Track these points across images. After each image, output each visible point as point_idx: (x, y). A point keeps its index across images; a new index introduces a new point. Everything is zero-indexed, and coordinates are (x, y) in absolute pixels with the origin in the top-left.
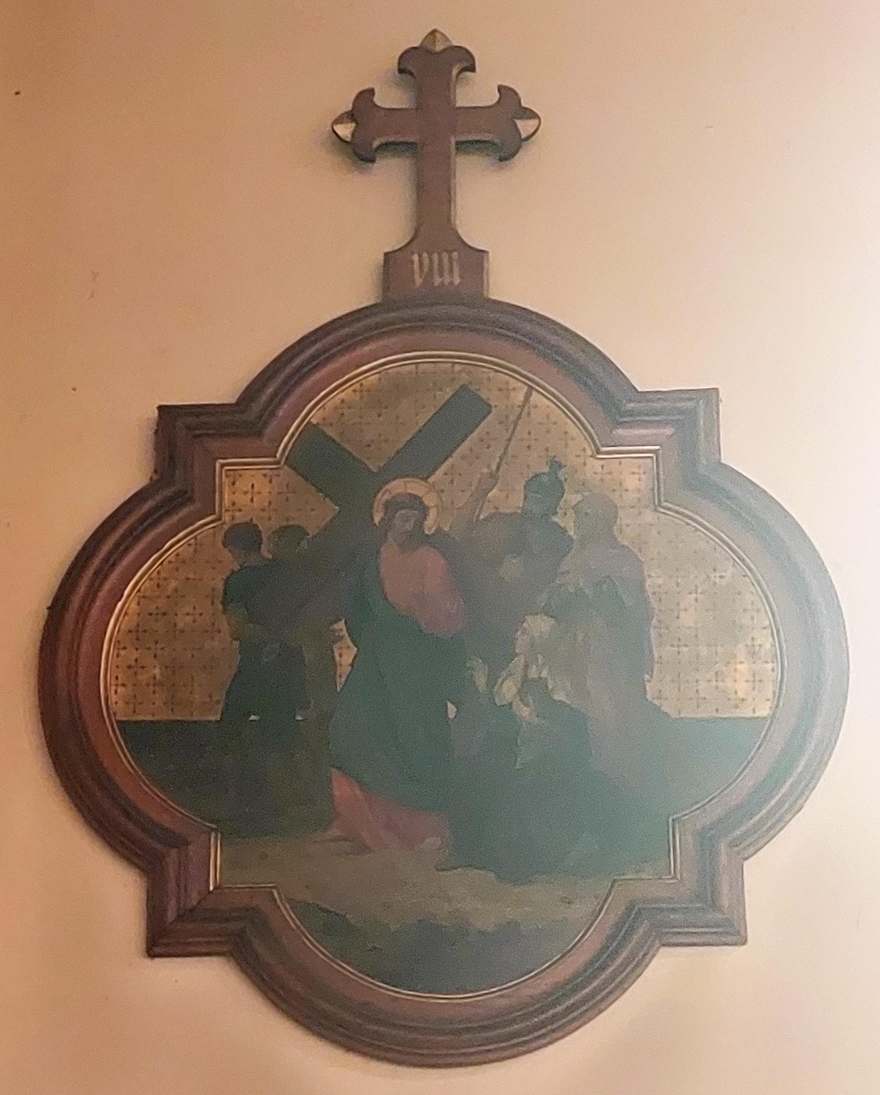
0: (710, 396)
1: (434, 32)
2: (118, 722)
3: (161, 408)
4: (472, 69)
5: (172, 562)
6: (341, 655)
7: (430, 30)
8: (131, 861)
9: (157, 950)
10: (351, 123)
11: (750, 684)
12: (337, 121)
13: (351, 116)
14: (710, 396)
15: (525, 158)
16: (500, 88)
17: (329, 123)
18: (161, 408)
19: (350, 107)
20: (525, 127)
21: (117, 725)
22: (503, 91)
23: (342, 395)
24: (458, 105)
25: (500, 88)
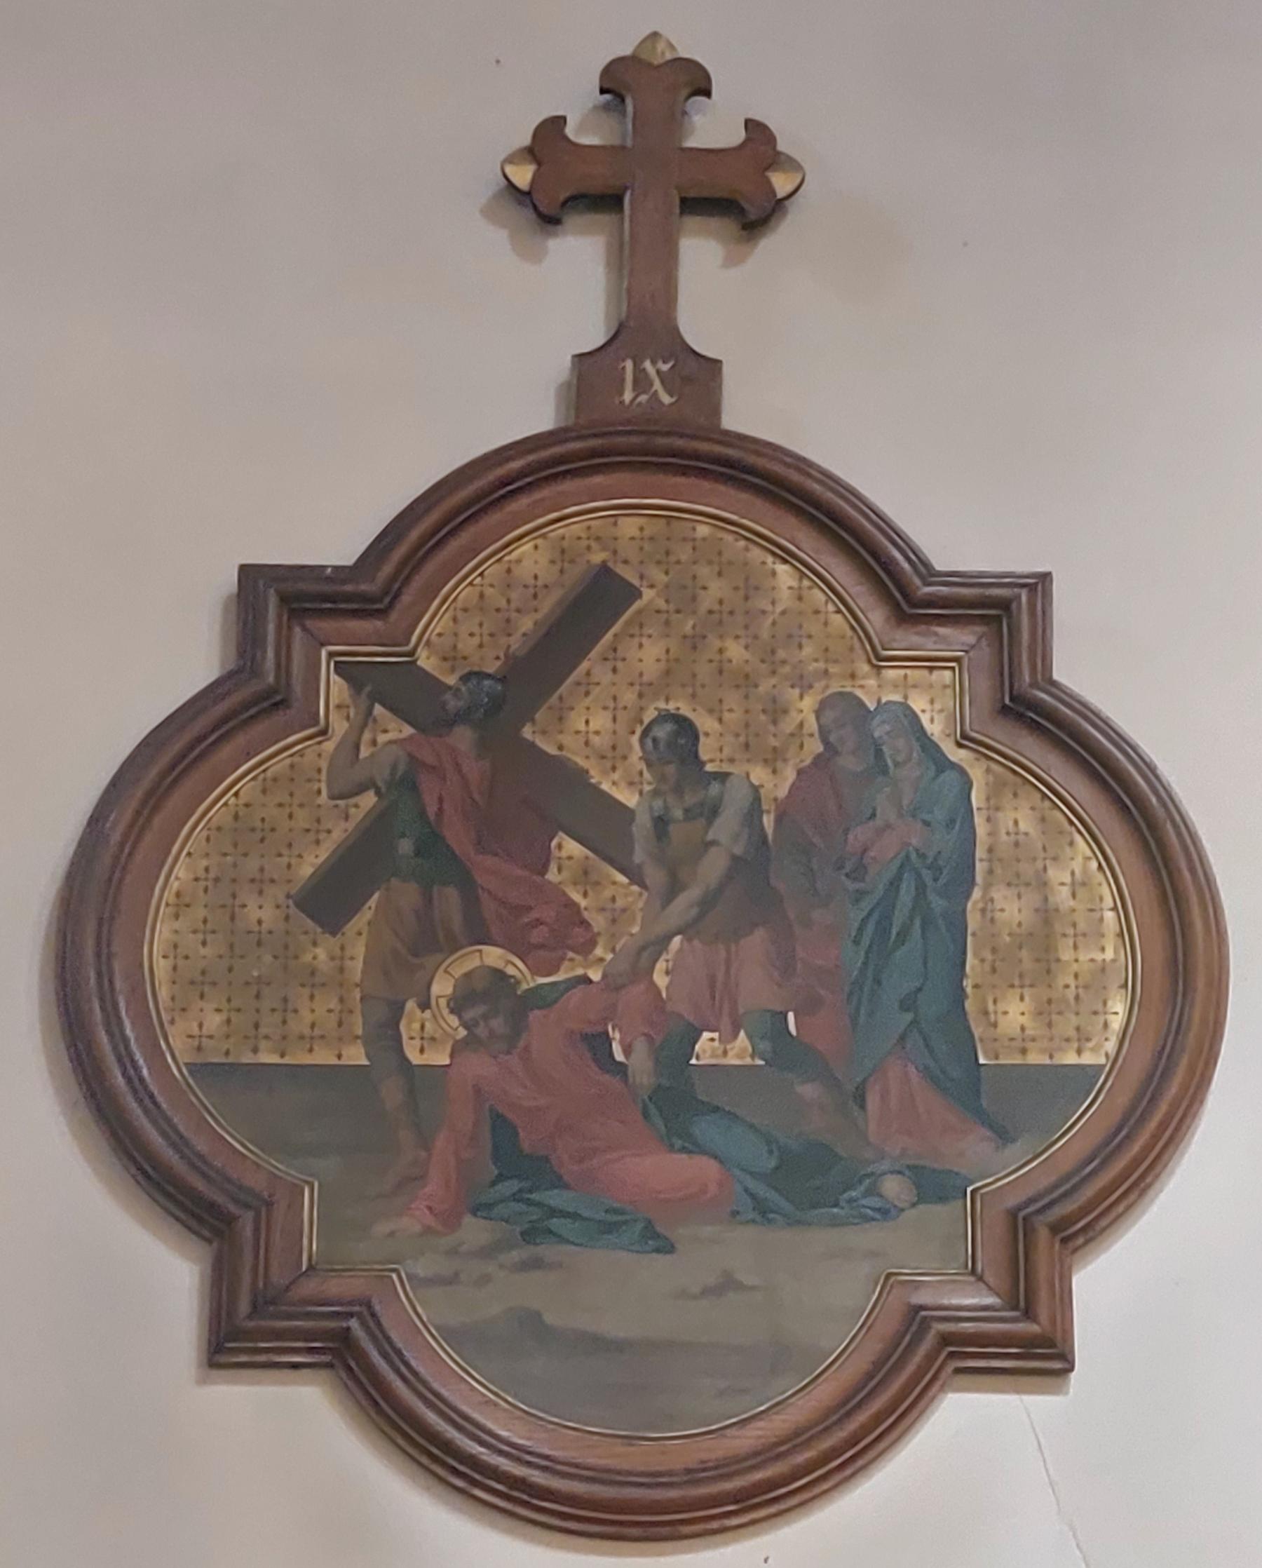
0: (1040, 584)
1: (655, 35)
2: (186, 1064)
3: (244, 569)
4: (707, 93)
5: (210, 983)
6: (995, 1002)
7: (648, 32)
8: (226, 694)
9: (223, 1359)
10: (530, 163)
11: (316, 993)
12: (510, 160)
13: (531, 153)
14: (1040, 584)
15: (771, 244)
16: (748, 123)
17: (503, 157)
18: (244, 569)
19: (526, 140)
20: (781, 183)
21: (187, 1068)
22: (750, 125)
23: (561, 531)
24: (691, 143)
25: (748, 123)
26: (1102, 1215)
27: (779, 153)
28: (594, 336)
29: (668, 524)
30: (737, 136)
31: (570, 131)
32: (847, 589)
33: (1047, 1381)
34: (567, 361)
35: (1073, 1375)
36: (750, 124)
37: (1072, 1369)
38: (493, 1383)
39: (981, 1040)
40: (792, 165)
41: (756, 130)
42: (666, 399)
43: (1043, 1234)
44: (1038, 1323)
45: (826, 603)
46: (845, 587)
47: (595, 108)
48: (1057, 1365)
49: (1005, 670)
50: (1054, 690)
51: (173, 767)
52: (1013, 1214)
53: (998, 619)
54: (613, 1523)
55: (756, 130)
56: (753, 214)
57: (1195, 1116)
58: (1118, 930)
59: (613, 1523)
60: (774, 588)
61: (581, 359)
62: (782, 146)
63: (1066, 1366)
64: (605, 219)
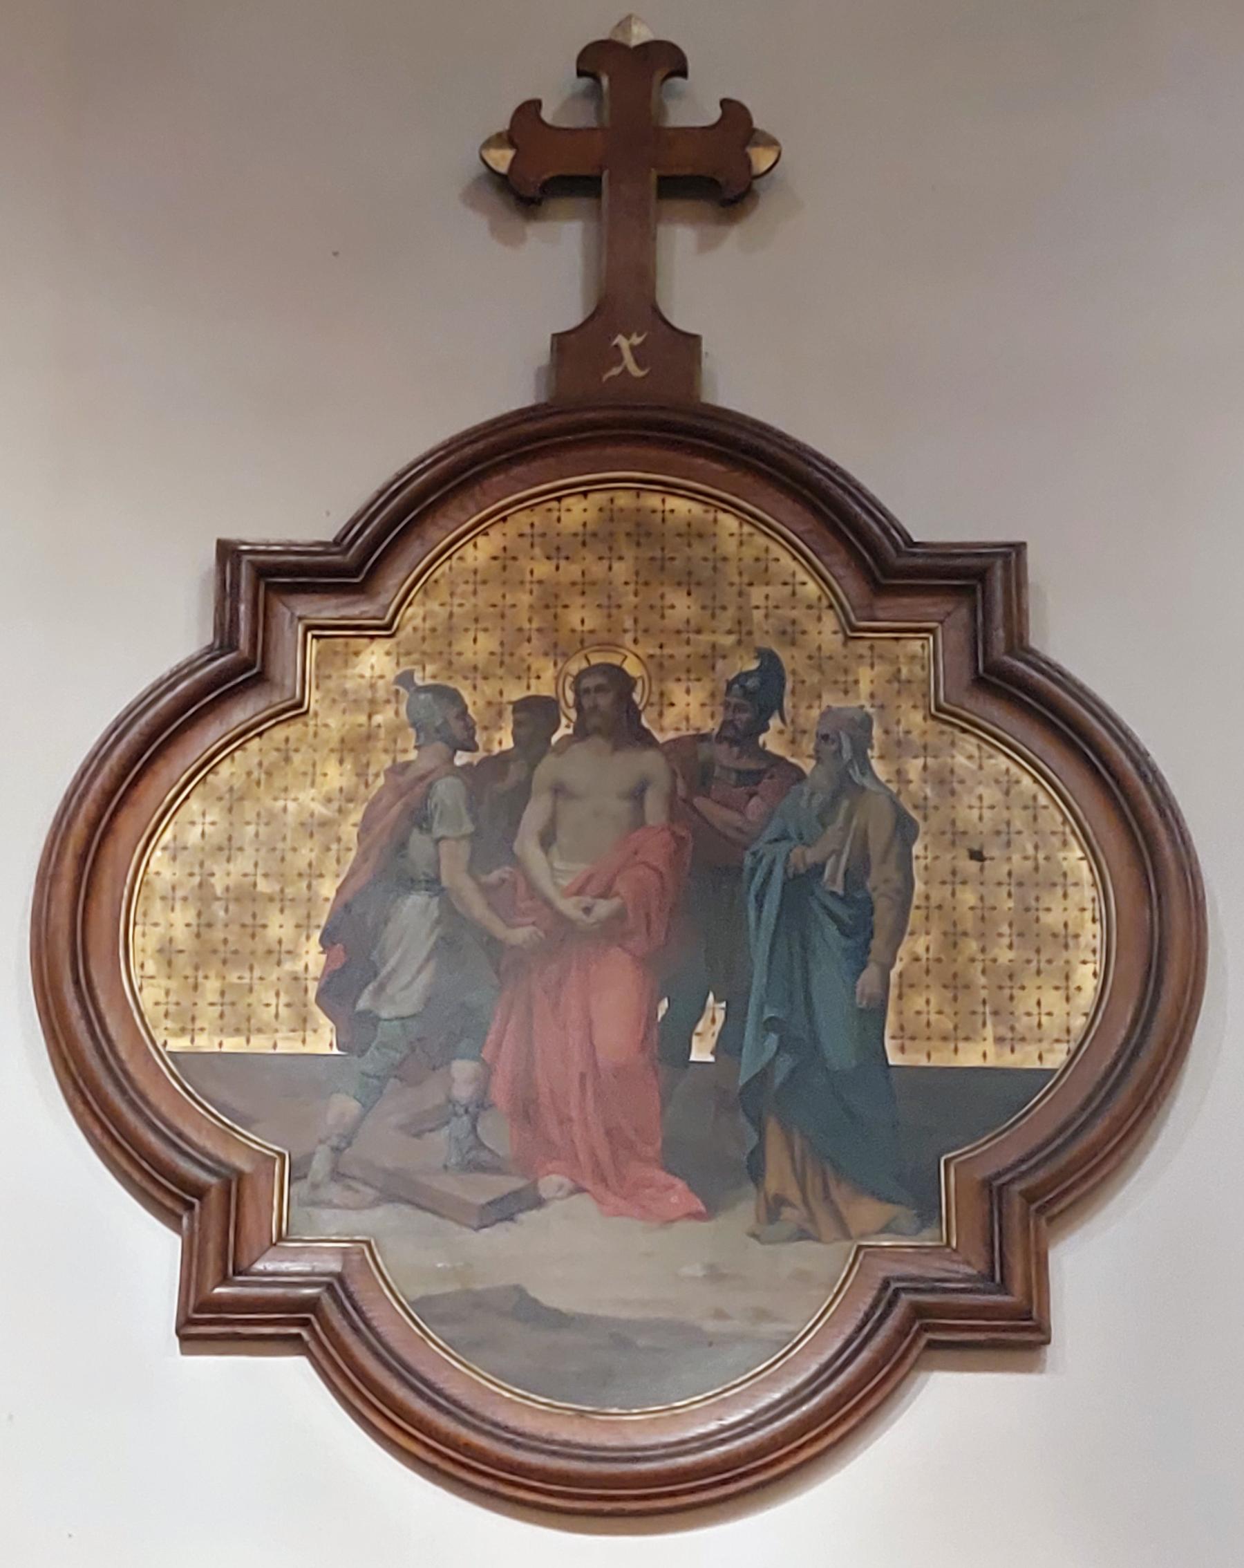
4: (683, 73)
12: (488, 144)
13: (507, 139)
26: (1085, 1177)
27: (754, 131)
28: (571, 315)
29: (638, 496)
30: (713, 114)
31: (547, 115)
32: (1059, 775)
33: (1018, 1356)
34: (546, 344)
35: (1049, 1349)
36: (725, 103)
37: (1048, 1342)
38: (517, 1387)
39: (176, 823)
40: (772, 142)
41: (733, 111)
42: (636, 372)
43: (1016, 1206)
44: (1013, 1295)
45: (741, 525)
46: (1026, 744)
47: (574, 97)
48: (1042, 1338)
49: (978, 639)
50: (1030, 657)
51: (126, 770)
52: (987, 1183)
53: (973, 590)
54: (856, 1408)
55: (733, 111)
56: (729, 195)
57: (1176, 1075)
58: (527, 512)
59: (856, 1408)
60: (715, 535)
61: (560, 341)
62: (758, 123)
63: (1042, 1338)
64: (585, 203)
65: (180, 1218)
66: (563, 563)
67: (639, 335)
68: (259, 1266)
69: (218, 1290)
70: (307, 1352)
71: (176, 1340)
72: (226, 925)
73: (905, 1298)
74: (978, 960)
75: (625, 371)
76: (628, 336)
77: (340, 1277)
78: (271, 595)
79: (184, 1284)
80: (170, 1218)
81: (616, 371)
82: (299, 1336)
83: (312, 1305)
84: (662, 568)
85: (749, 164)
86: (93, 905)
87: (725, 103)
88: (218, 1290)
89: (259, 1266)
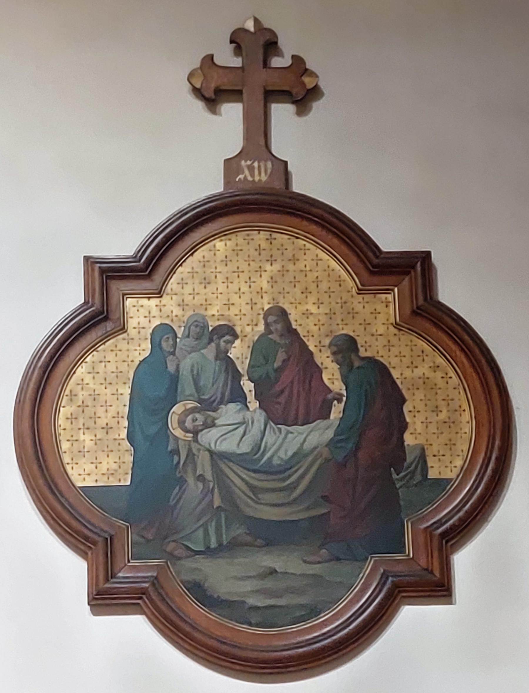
36: (293, 57)
41: (297, 60)
55: (297, 60)
65: (86, 554)
66: (230, 285)
67: (250, 161)
68: (120, 575)
69: (107, 585)
70: (144, 613)
71: (88, 608)
72: (96, 451)
73: (390, 579)
74: (260, 178)
75: (245, 177)
76: (246, 161)
77: (156, 578)
78: (101, 309)
79: (86, 294)
80: (83, 555)
81: (241, 176)
82: (138, 604)
83: (144, 592)
84: (280, 293)
85: (303, 84)
86: (41, 406)
87: (293, 57)
88: (107, 585)
89: (120, 575)
